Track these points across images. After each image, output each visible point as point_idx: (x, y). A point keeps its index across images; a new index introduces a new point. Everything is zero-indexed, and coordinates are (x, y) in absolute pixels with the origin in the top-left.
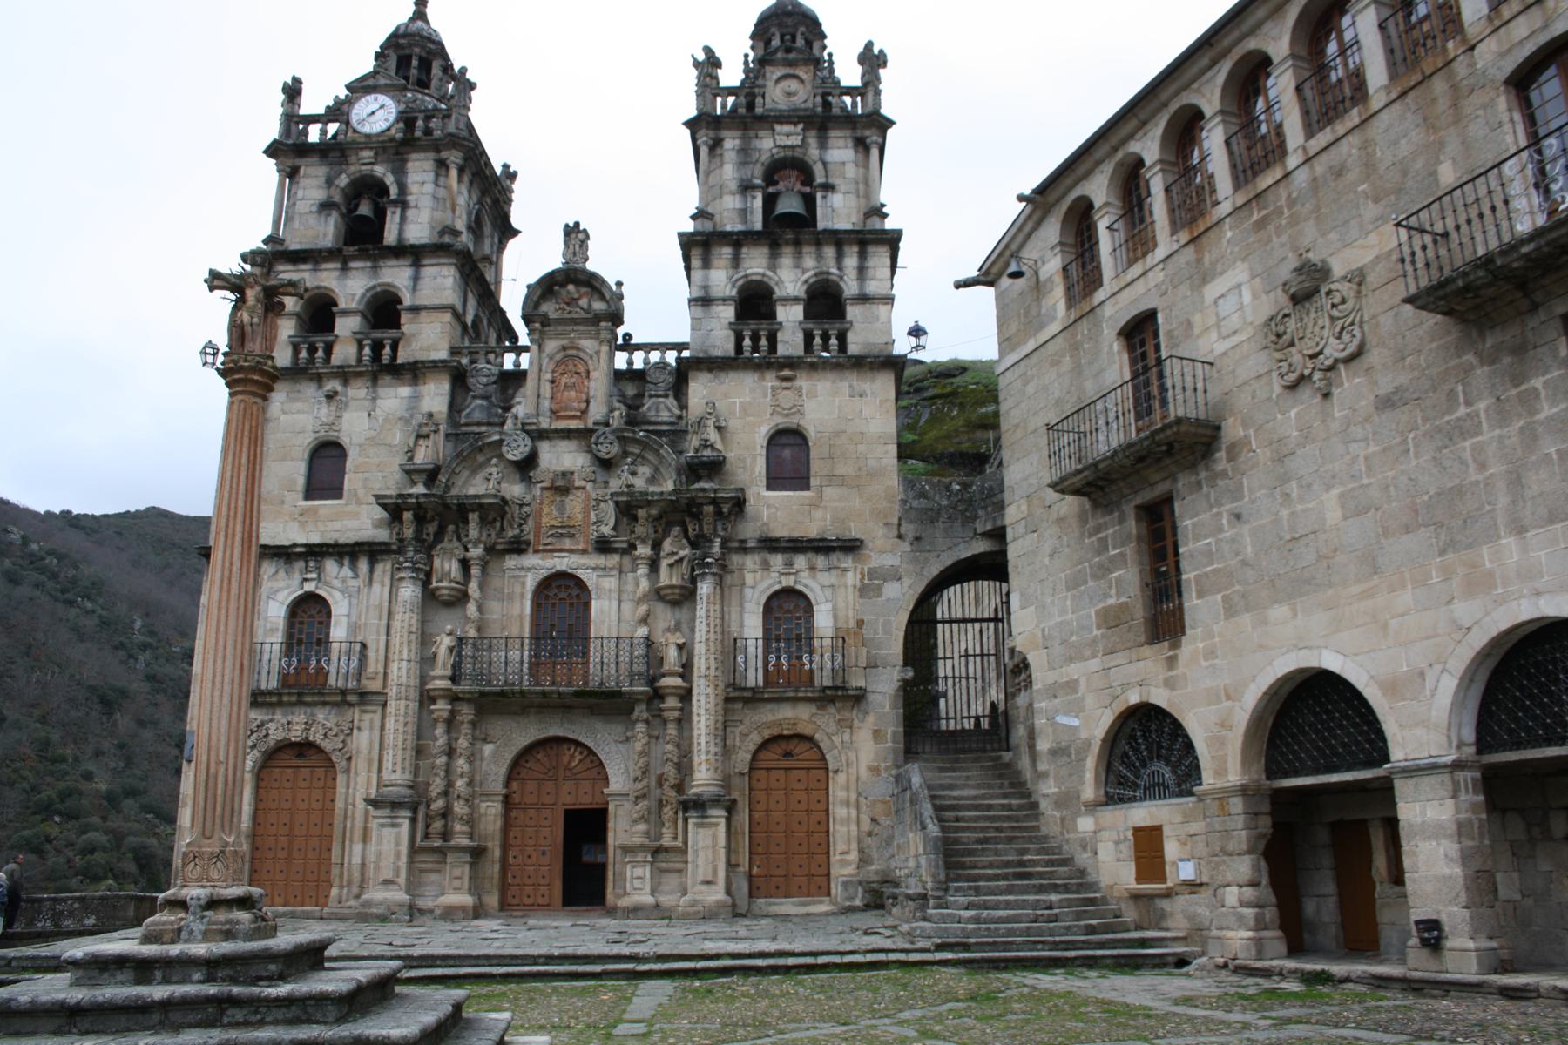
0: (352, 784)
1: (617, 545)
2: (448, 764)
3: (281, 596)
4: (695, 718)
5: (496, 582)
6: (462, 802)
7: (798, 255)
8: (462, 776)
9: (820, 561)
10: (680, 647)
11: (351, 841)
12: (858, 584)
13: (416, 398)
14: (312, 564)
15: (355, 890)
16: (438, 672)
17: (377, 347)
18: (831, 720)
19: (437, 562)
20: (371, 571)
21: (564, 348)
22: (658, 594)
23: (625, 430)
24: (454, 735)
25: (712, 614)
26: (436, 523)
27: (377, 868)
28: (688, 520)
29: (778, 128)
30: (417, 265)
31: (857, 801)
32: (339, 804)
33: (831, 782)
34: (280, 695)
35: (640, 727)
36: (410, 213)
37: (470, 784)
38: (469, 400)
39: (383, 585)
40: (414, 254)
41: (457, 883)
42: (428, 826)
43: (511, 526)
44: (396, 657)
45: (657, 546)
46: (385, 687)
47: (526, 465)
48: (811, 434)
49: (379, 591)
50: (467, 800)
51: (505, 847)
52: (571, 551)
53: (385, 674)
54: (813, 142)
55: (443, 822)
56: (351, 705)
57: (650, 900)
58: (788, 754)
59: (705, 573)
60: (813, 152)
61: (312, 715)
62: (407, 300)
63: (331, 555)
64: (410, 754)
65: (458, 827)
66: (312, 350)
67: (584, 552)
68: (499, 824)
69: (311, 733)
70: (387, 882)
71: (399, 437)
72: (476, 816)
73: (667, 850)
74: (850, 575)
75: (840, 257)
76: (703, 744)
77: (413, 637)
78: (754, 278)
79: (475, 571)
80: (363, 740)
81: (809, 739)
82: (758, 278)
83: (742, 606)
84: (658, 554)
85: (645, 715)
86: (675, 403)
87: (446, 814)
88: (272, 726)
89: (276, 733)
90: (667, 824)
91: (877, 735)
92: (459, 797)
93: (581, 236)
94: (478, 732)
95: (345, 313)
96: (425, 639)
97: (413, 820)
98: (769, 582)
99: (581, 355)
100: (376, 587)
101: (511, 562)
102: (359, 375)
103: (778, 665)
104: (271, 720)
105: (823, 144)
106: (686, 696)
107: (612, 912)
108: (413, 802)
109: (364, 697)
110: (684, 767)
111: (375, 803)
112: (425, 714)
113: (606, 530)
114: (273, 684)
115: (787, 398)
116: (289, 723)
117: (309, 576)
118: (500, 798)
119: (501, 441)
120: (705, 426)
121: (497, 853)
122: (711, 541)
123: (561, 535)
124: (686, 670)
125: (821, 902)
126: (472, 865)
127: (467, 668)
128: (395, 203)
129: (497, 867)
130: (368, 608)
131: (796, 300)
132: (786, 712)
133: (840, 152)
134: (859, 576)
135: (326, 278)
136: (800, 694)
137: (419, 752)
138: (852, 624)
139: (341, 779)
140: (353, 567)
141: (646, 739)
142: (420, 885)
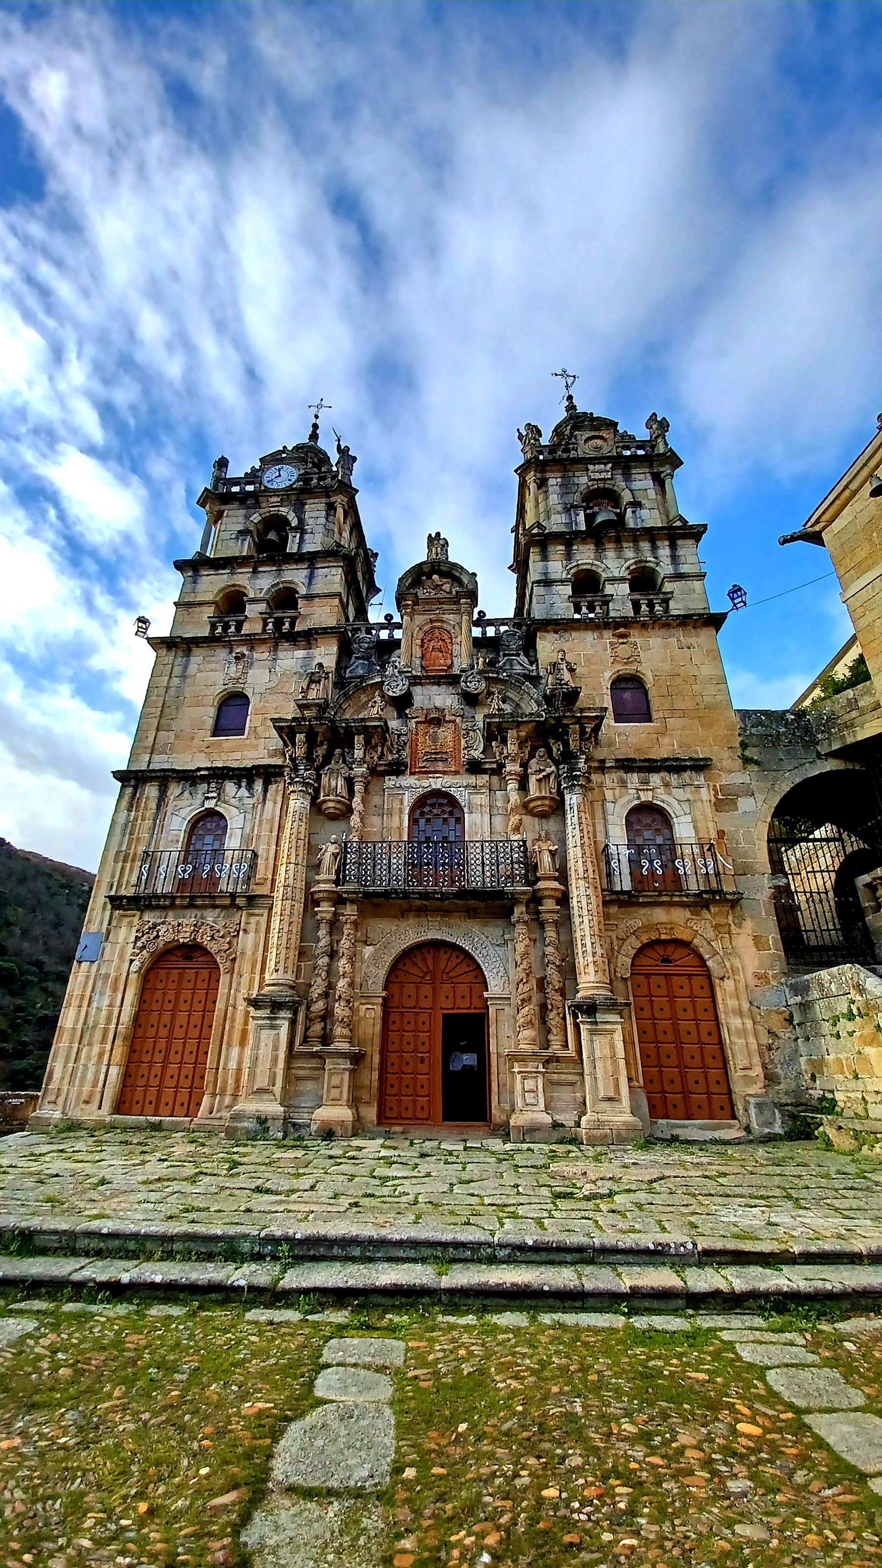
0: (234, 985)
1: (487, 766)
2: (329, 965)
3: (183, 813)
4: (577, 920)
5: (376, 800)
6: (343, 1003)
7: (619, 549)
8: (344, 975)
9: (674, 779)
10: (553, 854)
11: (229, 1045)
12: (713, 799)
13: (310, 658)
14: (213, 785)
15: (227, 1100)
16: (323, 877)
17: (279, 623)
18: (708, 926)
19: (325, 780)
20: (265, 791)
21: (431, 621)
22: (526, 807)
23: (488, 672)
24: (335, 937)
25: (584, 821)
26: (325, 747)
27: (252, 1075)
28: (551, 741)
29: (591, 467)
30: (312, 568)
31: (750, 1010)
32: (220, 1005)
33: (718, 988)
34: (173, 898)
35: (521, 929)
36: (307, 536)
37: (351, 985)
38: (353, 659)
39: (275, 803)
40: (311, 560)
41: (335, 1093)
42: (307, 1029)
43: (391, 752)
44: (284, 860)
45: (525, 765)
46: (272, 891)
47: (402, 703)
48: (649, 679)
49: (272, 808)
50: (348, 1002)
51: (384, 1052)
52: (444, 773)
53: (273, 881)
54: (619, 477)
55: (322, 1024)
56: (240, 908)
57: (547, 1119)
58: (666, 960)
59: (574, 785)
60: (620, 483)
61: (202, 917)
62: (303, 591)
63: (231, 778)
64: (293, 953)
65: (338, 1030)
66: (226, 627)
67: (456, 773)
68: (378, 1027)
69: (200, 934)
70: (261, 1091)
71: (294, 687)
72: (355, 1018)
73: (558, 1060)
74: (704, 791)
75: (654, 548)
76: (589, 945)
77: (301, 843)
78: (585, 567)
79: (358, 787)
80: (248, 942)
81: (685, 944)
82: (588, 567)
83: (605, 819)
84: (526, 770)
85: (526, 917)
86: (526, 660)
87: (327, 1015)
88: (163, 929)
89: (166, 934)
90: (554, 1031)
91: (758, 942)
92: (340, 997)
93: (442, 542)
94: (359, 934)
95: (254, 601)
96: (312, 849)
97: (293, 1023)
98: (628, 798)
99: (445, 626)
100: (269, 804)
101: (390, 781)
102: (263, 641)
103: (652, 871)
104: (163, 923)
105: (627, 477)
106: (564, 900)
107: (504, 1131)
108: (293, 1002)
109: (252, 900)
110: (569, 971)
111: (255, 1003)
112: (308, 919)
113: (477, 754)
114: (168, 889)
115: (624, 650)
116: (179, 925)
117: (210, 795)
118: (380, 1000)
119: (382, 682)
120: (559, 670)
121: (376, 1059)
122: (577, 758)
123: (436, 760)
124: (562, 875)
125: (730, 1127)
126: (352, 1072)
127: (352, 870)
128: (295, 529)
129: (375, 1075)
130: (261, 821)
131: (622, 580)
132: (659, 915)
133: (643, 482)
134: (712, 793)
135: (242, 578)
136: (676, 899)
137: (302, 954)
138: (713, 835)
139: (224, 979)
140: (250, 787)
141: (527, 942)
142: (298, 1094)
